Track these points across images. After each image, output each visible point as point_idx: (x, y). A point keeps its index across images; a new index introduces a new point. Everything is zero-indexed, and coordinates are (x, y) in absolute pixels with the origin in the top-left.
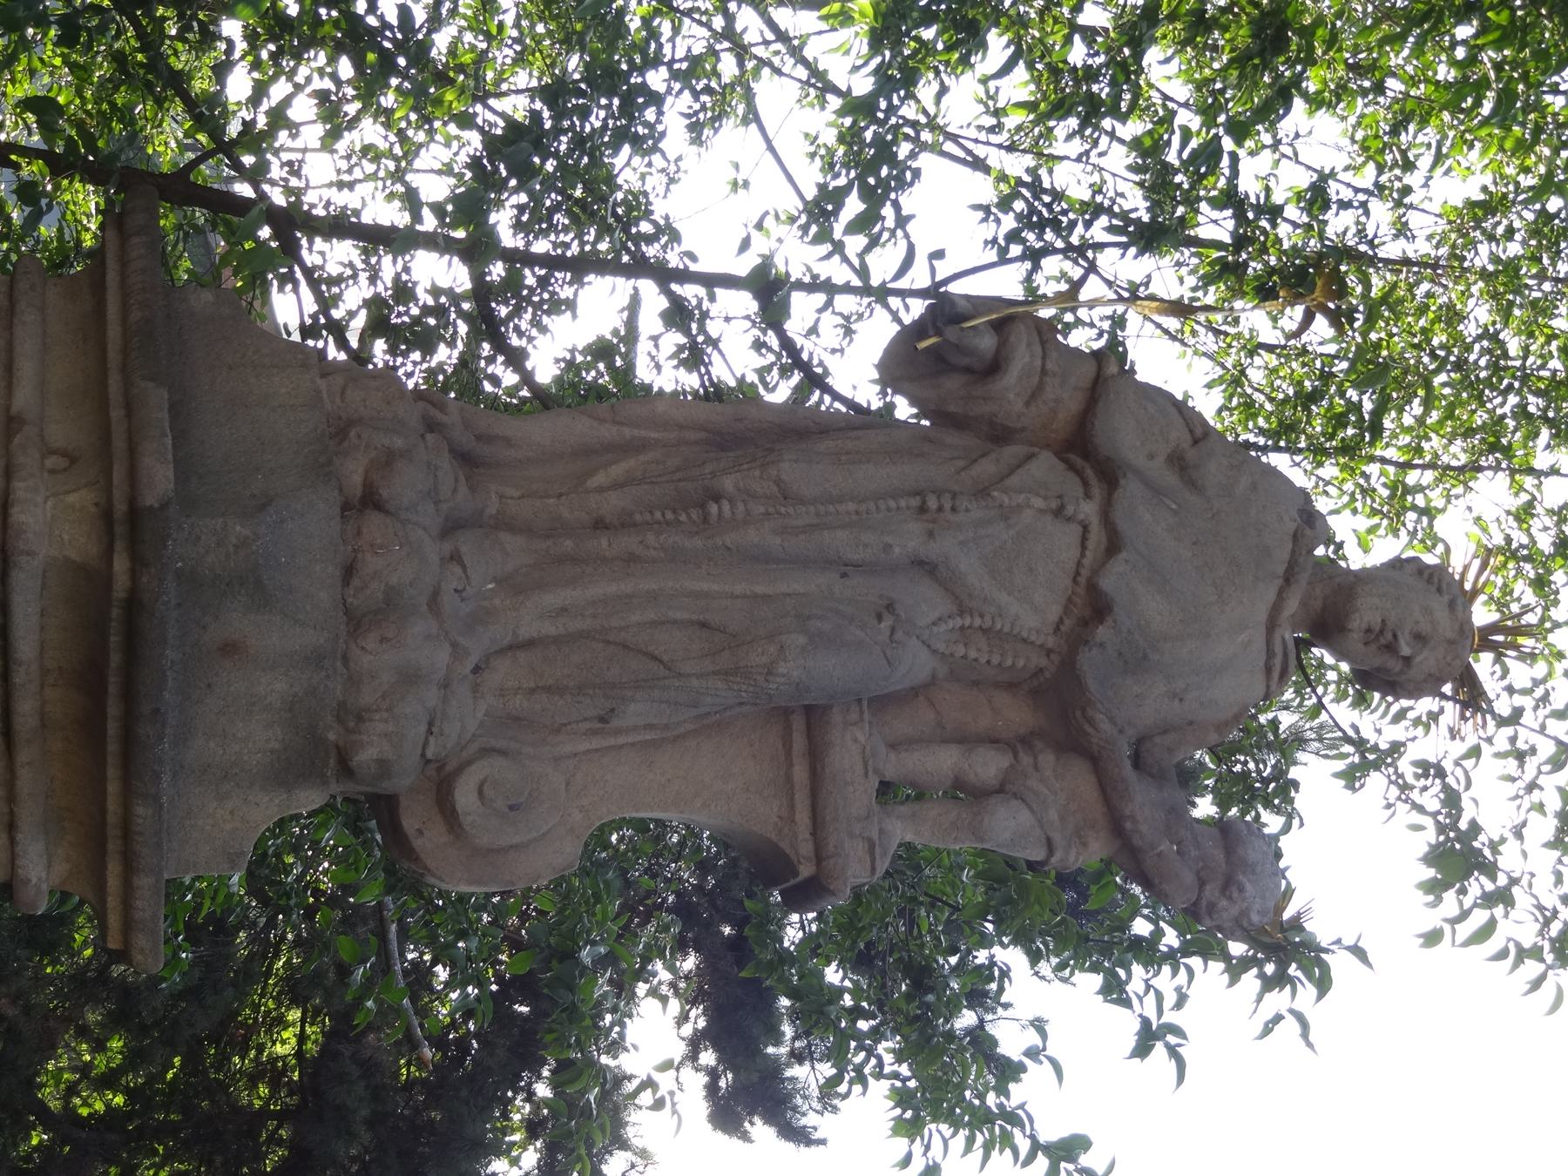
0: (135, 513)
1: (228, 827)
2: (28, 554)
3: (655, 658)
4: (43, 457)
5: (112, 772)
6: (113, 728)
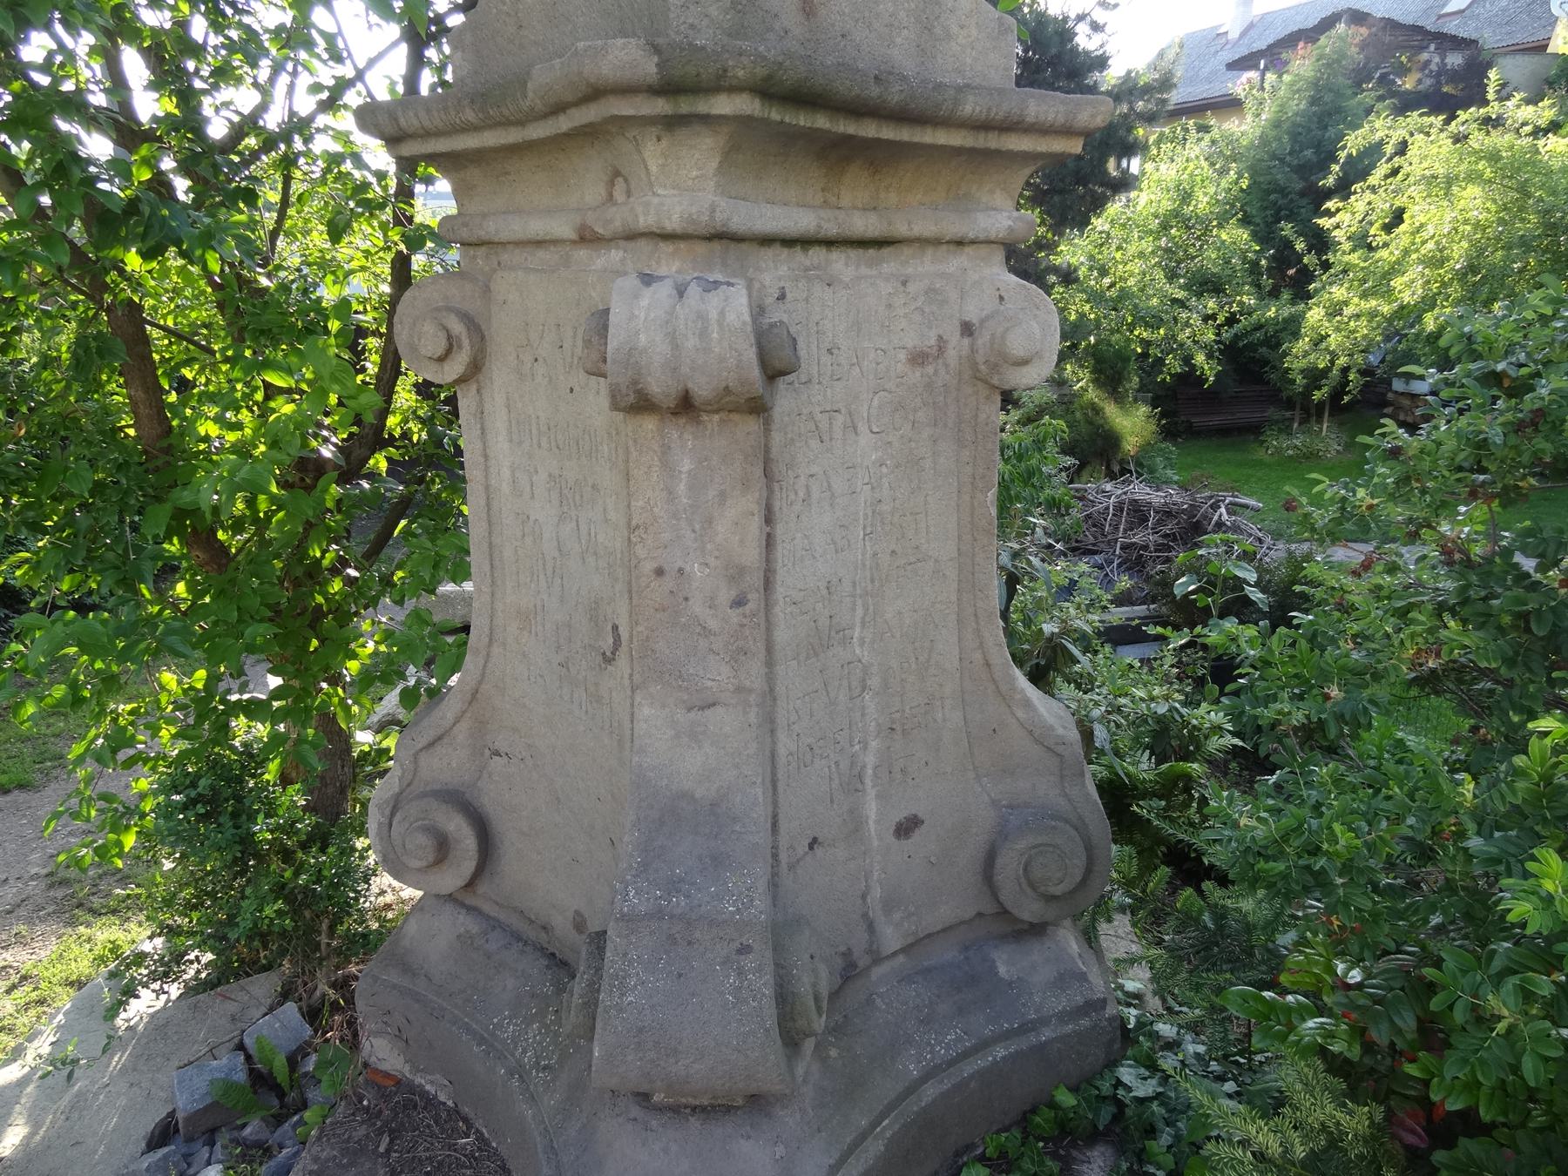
0: (668, 88)
1: (974, 32)
3: (431, 745)
4: (616, 204)
5: (928, 136)
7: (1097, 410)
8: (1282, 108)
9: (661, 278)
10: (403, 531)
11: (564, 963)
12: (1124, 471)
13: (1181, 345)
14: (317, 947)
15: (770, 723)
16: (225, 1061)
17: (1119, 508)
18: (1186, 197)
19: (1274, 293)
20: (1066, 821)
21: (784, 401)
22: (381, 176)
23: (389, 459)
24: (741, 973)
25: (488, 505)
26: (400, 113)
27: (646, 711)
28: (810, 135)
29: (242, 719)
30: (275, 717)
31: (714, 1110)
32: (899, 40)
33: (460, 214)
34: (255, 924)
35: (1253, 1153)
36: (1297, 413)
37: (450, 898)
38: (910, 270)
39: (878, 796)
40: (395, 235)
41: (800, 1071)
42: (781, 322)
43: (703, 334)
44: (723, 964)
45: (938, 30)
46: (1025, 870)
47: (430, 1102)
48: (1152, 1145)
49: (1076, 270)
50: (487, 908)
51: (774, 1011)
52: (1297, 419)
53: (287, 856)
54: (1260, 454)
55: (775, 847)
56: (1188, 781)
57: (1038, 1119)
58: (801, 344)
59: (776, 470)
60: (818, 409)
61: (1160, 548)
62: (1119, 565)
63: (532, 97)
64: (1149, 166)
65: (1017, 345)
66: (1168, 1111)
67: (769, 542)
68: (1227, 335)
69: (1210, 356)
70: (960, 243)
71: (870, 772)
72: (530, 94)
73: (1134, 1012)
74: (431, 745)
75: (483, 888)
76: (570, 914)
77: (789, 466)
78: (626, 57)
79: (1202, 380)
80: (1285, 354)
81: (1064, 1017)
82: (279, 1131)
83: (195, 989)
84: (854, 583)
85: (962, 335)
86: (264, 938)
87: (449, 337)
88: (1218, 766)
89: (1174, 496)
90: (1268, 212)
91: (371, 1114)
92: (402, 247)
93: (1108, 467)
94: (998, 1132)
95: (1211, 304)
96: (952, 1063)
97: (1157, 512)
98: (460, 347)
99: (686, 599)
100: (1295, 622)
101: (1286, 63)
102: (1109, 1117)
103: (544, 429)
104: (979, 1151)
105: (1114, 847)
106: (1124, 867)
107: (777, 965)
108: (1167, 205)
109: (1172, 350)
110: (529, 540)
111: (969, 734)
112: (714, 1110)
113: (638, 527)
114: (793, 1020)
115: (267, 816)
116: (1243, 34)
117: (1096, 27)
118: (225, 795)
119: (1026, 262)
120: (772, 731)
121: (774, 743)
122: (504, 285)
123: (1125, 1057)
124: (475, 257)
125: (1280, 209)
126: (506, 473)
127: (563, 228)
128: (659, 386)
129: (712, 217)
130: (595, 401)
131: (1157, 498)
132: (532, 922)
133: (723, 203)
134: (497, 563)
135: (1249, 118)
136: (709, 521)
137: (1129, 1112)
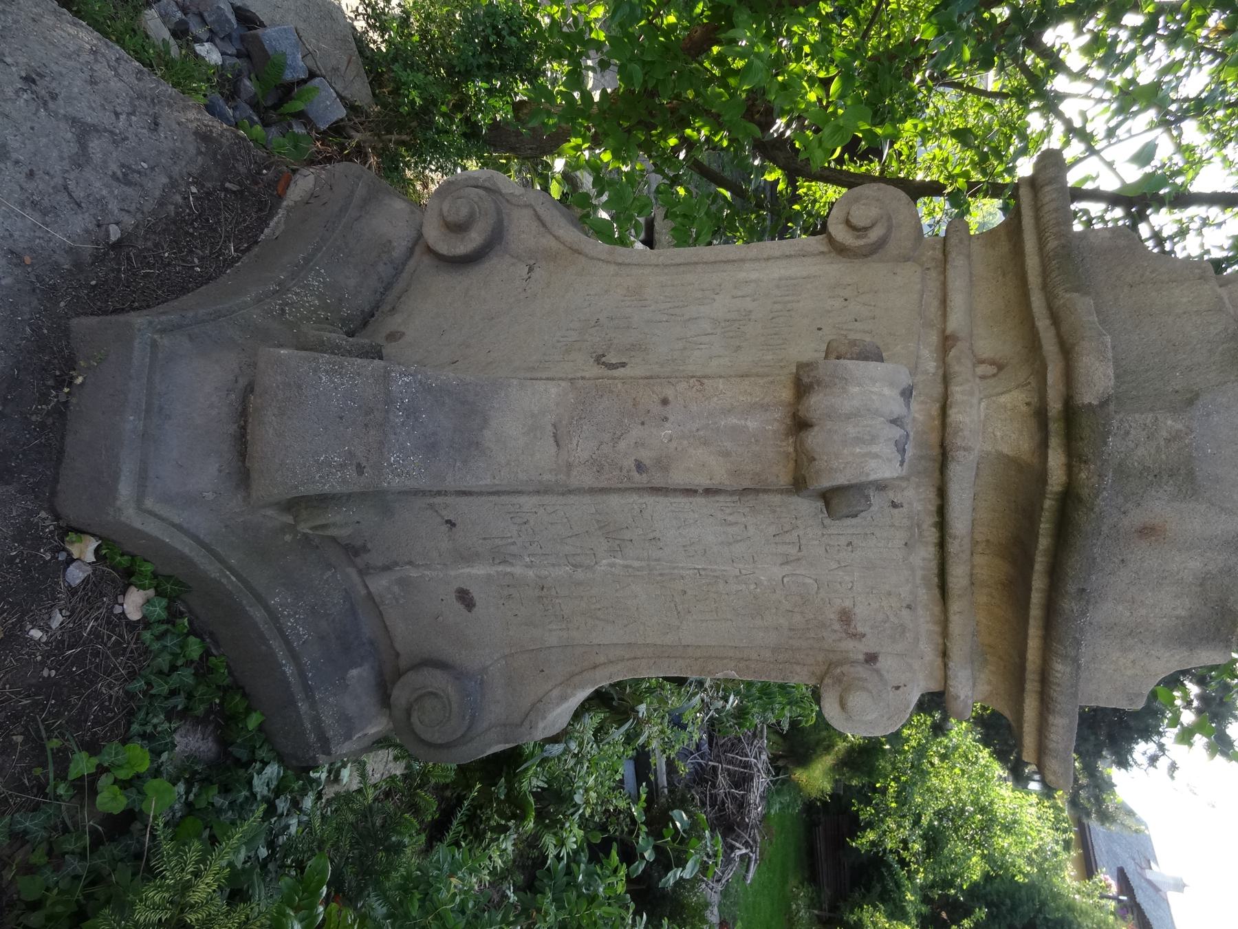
0: (1071, 412)
1: (1129, 673)
2: (965, 449)
4: (974, 366)
6: (1036, 598)
7: (829, 748)
8: (1084, 913)
9: (908, 405)
10: (718, 195)
11: (362, 327)
12: (778, 770)
13: (882, 821)
14: (389, 132)
15: (543, 490)
16: (301, 63)
17: (747, 765)
18: (1008, 829)
19: (926, 900)
20: (469, 728)
21: (806, 507)
22: (1010, 171)
23: (777, 182)
24: (342, 466)
25: (728, 261)
26: (1054, 186)
27: (554, 391)
28: (1033, 534)
29: (566, 69)
30: (567, 96)
31: (242, 443)
32: (1120, 608)
33: (971, 236)
34: (404, 84)
35: (190, 880)
36: (828, 914)
37: (420, 235)
38: (920, 612)
39: (490, 575)
40: (961, 182)
41: (270, 512)
42: (870, 505)
43: (858, 440)
44: (350, 452)
45: (1130, 641)
46: (431, 693)
47: (263, 222)
48: (215, 790)
49: (945, 735)
50: (412, 263)
51: (312, 493)
52: (823, 913)
53: (459, 106)
54: (793, 882)
55: (446, 493)
56: (521, 818)
57: (238, 698)
58: (854, 521)
59: (750, 497)
60: (801, 533)
61: (714, 798)
62: (700, 764)
63: (1065, 297)
64: (1034, 799)
65: (857, 700)
66: (241, 804)
67: (690, 492)
68: (891, 858)
69: (873, 843)
70: (944, 654)
71: (509, 569)
72: (1068, 295)
73: (324, 776)
74: (538, 218)
75: (427, 260)
76: (402, 329)
77: (752, 508)
78: (1097, 377)
79: (854, 837)
80: (875, 907)
81: (317, 721)
82: (247, 107)
83: (360, 41)
84: (658, 560)
85: (866, 654)
86: (396, 92)
87: (866, 229)
88: (533, 842)
89: (757, 810)
90: (995, 898)
91: (255, 177)
92: (949, 189)
93: (781, 757)
94: (228, 667)
95: (917, 846)
96: (281, 632)
97: (743, 796)
98: (858, 237)
99: (643, 424)
100: (638, 918)
101: (1124, 918)
102: (238, 755)
103: (789, 306)
104: (214, 651)
105: (454, 766)
106: (438, 771)
107: (350, 495)
108: (1000, 812)
109: (877, 813)
110: (699, 294)
111: (540, 650)
112: (242, 443)
113: (702, 384)
114: (306, 508)
115: (486, 90)
116: (1149, 882)
117: (1153, 760)
118: (505, 58)
119: (935, 703)
120: (538, 492)
121: (529, 493)
122: (909, 274)
123: (286, 768)
124: (934, 249)
125: (997, 907)
126: (754, 276)
127: (956, 321)
128: (816, 403)
129: (959, 448)
130: (808, 349)
131: (755, 797)
132: (399, 298)
133: (972, 457)
134: (682, 269)
135: (1076, 884)
136: (705, 443)
137: (241, 772)
